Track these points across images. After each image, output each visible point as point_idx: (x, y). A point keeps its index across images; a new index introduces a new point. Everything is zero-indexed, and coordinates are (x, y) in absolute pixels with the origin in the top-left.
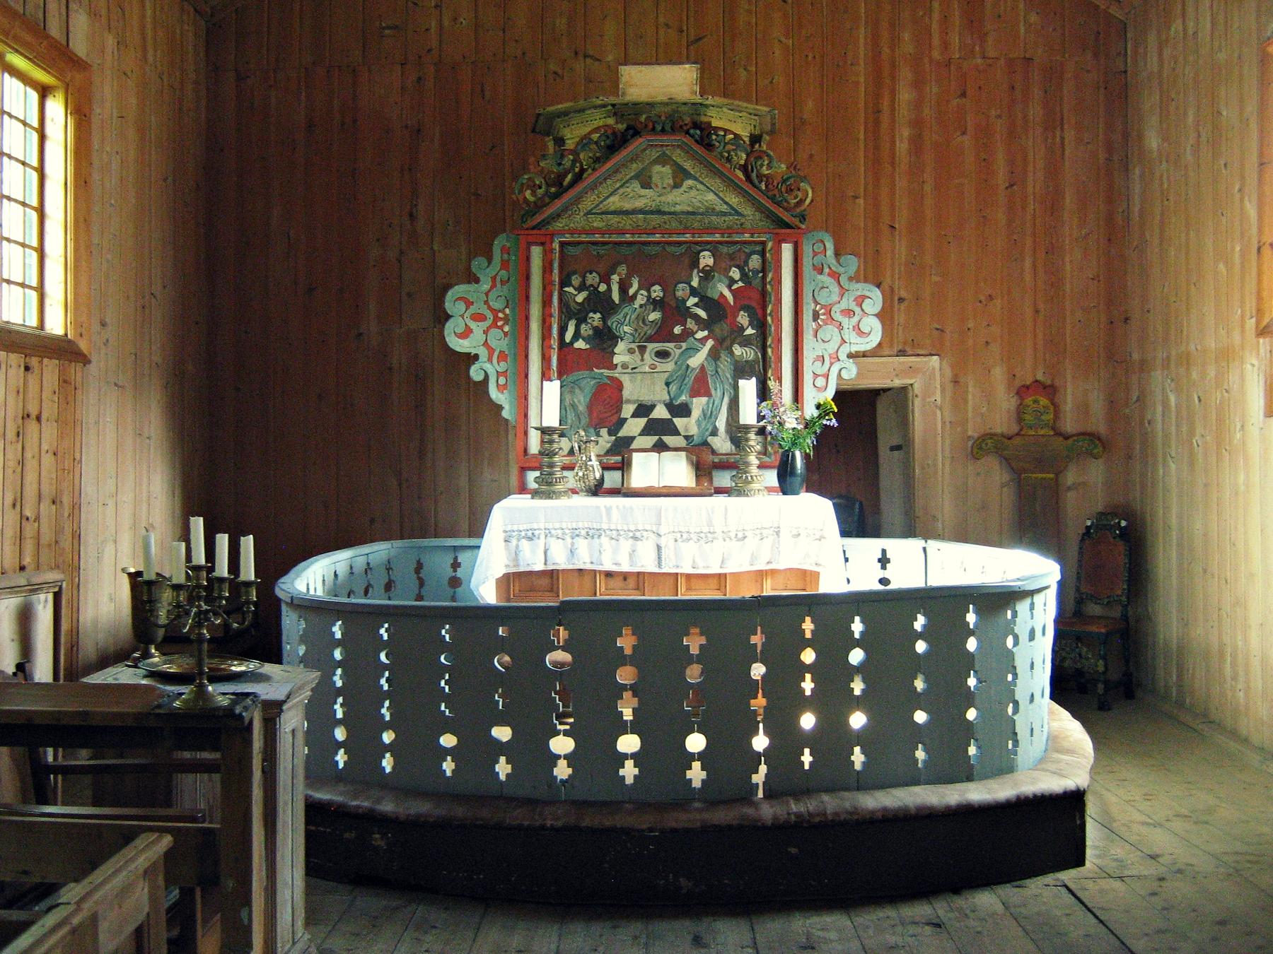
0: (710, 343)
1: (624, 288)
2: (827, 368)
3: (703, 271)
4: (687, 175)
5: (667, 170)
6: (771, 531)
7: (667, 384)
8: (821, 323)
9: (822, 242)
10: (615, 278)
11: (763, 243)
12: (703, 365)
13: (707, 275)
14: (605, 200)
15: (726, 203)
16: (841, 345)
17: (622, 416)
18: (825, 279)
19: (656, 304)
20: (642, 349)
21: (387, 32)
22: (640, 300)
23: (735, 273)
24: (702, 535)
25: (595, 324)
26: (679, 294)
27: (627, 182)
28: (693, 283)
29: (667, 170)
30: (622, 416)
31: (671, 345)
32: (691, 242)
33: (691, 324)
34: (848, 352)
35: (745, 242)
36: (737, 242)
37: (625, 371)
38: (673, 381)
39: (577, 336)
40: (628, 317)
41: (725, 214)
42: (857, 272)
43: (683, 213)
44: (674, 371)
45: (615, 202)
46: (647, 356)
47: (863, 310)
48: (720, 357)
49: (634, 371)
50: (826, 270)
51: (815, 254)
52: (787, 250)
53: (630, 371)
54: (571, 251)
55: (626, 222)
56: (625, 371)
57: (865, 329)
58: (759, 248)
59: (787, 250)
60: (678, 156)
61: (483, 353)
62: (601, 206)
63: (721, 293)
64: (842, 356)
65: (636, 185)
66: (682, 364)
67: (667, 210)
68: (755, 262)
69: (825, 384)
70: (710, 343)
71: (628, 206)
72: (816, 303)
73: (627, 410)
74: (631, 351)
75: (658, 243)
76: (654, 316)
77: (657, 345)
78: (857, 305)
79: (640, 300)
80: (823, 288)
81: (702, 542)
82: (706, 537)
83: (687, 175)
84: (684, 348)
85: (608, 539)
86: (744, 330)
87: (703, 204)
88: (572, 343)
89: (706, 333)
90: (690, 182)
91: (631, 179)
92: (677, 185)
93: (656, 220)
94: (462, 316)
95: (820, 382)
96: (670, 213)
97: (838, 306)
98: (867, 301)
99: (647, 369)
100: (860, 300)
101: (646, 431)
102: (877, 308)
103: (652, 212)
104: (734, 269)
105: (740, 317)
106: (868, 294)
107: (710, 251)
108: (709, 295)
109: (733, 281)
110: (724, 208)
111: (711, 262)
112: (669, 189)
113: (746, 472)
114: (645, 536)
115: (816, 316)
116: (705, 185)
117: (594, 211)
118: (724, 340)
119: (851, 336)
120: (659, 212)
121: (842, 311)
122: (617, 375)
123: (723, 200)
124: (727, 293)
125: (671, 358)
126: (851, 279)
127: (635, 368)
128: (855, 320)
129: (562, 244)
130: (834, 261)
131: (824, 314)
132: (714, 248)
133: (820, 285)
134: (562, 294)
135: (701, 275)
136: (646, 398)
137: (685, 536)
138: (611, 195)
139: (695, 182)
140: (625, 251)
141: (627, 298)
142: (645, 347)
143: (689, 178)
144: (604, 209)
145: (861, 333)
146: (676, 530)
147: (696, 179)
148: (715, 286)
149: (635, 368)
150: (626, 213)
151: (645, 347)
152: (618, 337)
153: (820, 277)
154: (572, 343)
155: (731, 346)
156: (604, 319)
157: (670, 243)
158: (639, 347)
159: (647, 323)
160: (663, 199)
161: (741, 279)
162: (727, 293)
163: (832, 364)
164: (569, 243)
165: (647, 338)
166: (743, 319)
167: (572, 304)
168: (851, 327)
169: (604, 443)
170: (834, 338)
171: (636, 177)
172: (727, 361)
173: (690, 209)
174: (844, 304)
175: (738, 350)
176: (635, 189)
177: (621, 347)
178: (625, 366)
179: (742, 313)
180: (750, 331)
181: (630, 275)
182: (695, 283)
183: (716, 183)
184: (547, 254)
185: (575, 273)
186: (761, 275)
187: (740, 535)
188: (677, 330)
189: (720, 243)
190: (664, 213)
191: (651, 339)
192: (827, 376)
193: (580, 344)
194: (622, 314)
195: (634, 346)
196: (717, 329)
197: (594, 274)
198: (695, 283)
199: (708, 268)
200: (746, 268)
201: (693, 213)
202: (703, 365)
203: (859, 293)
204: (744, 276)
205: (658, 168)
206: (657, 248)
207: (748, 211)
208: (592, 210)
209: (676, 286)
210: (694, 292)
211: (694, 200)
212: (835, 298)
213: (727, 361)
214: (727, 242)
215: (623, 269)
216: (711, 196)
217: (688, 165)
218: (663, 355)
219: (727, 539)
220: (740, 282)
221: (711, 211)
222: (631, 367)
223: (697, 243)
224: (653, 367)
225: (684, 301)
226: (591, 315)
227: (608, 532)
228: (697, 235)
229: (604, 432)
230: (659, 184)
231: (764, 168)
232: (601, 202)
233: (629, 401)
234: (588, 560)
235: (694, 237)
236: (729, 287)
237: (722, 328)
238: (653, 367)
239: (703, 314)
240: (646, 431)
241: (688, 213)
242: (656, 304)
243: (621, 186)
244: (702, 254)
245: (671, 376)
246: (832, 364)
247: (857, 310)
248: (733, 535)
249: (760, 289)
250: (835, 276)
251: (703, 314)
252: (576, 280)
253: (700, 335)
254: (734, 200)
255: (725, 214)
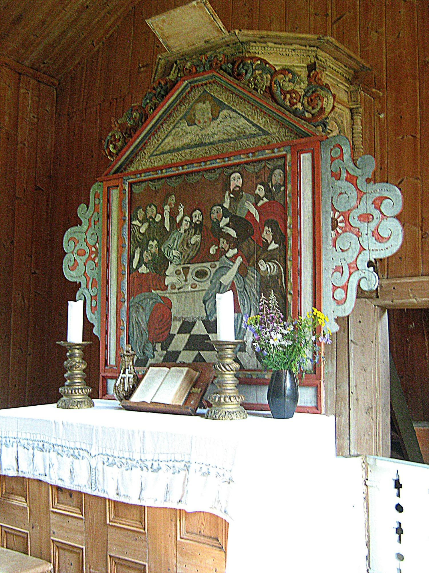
0: (239, 260)
1: (173, 218)
2: (346, 280)
3: (233, 192)
4: (222, 106)
5: (207, 105)
6: (181, 465)
7: (205, 302)
8: (340, 231)
9: (340, 146)
10: (167, 208)
11: (284, 157)
12: (233, 282)
13: (237, 196)
14: (162, 142)
15: (254, 125)
16: (360, 253)
17: (171, 333)
18: (343, 184)
19: (196, 228)
20: (186, 270)
21: (142, 69)
22: (185, 226)
23: (260, 191)
24: (124, 461)
25: (153, 250)
26: (214, 216)
27: (178, 122)
28: (225, 205)
29: (207, 105)
30: (171, 333)
31: (208, 265)
32: (223, 167)
33: (223, 243)
34: (367, 260)
35: (268, 159)
36: (260, 161)
37: (174, 291)
38: (210, 298)
39: (140, 264)
40: (176, 242)
41: (253, 136)
42: (374, 174)
43: (219, 141)
44: (210, 288)
45: (169, 142)
46: (189, 276)
47: (381, 212)
48: (247, 273)
49: (181, 290)
50: (344, 175)
51: (333, 160)
52: (306, 159)
53: (176, 291)
54: (136, 189)
55: (176, 158)
56: (174, 291)
57: (384, 234)
58: (280, 163)
59: (306, 159)
60: (215, 91)
61: (83, 280)
62: (160, 147)
63: (249, 211)
64: (362, 264)
65: (184, 124)
66: (215, 283)
67: (207, 141)
68: (277, 176)
69: (344, 296)
70: (239, 260)
71: (179, 144)
72: (334, 210)
73: (176, 326)
74: (178, 273)
75: (198, 172)
76: (195, 239)
77: (197, 265)
78: (375, 208)
79: (185, 226)
80: (341, 194)
81: (124, 468)
82: (127, 463)
83: (222, 106)
84: (217, 267)
85: (55, 453)
86: (268, 245)
87: (235, 130)
88: (137, 269)
89: (236, 251)
90: (225, 112)
91: (181, 119)
92: (215, 118)
93: (199, 152)
94: (72, 252)
95: (340, 294)
96: (210, 144)
97: (356, 210)
98: (385, 202)
99: (190, 289)
100: (378, 203)
101: (188, 347)
102: (398, 209)
103: (196, 146)
104: (259, 186)
105: (265, 233)
106: (386, 194)
107: (239, 172)
108: (238, 214)
109: (258, 198)
110: (253, 130)
111: (240, 182)
112: (208, 123)
113: (220, 393)
114: (82, 455)
115: (334, 225)
116: (237, 112)
117: (155, 153)
118: (251, 257)
119: (370, 243)
120: (202, 144)
121: (360, 217)
122: (167, 295)
123: (251, 122)
124: (253, 211)
125: (208, 277)
126: (368, 181)
127: (180, 288)
128: (373, 225)
129: (131, 185)
130: (351, 164)
131: (342, 222)
132: (241, 168)
133: (339, 191)
134: (130, 226)
135: (232, 196)
136: (189, 316)
137: (111, 459)
138: (167, 136)
139: (229, 111)
140: (174, 183)
141: (175, 225)
142: (188, 268)
143: (224, 109)
144: (161, 151)
145: (380, 239)
146: (104, 453)
147: (231, 109)
148: (243, 204)
149: (180, 288)
150: (178, 150)
151: (188, 268)
152: (168, 261)
153: (338, 183)
154: (137, 269)
155: (257, 262)
156: (159, 246)
157: (206, 170)
158: (183, 268)
159: (190, 245)
160: (203, 132)
161: (265, 196)
162: (253, 211)
163: (350, 274)
164: (134, 183)
165: (190, 260)
166: (267, 234)
167: (137, 234)
168: (370, 233)
169: (159, 357)
170: (353, 246)
171: (184, 117)
172: (254, 277)
173: (225, 137)
174: (362, 209)
175: (263, 266)
176: (184, 128)
177: (171, 269)
178: (173, 287)
179: (266, 228)
180: (273, 246)
181: (177, 205)
182: (226, 205)
183: (245, 109)
184: (122, 193)
185: (139, 208)
186: (282, 189)
187: (155, 467)
188: (212, 250)
189: (247, 163)
190: (205, 145)
191: (191, 261)
192: (345, 288)
193: (143, 269)
194: (172, 240)
195: (180, 268)
196: (244, 245)
197: (153, 207)
198: (226, 205)
199: (238, 189)
200: (270, 184)
201: (228, 140)
202: (233, 282)
203: (377, 195)
204: (268, 191)
205: (200, 105)
206: (198, 177)
207: (273, 129)
208: (153, 153)
209: (211, 210)
210: (226, 213)
211: (228, 128)
212: (354, 203)
213: (254, 277)
214: (253, 162)
215: (172, 200)
216: (242, 121)
217: (223, 98)
218: (201, 274)
219: (145, 468)
220: (264, 199)
221: (242, 135)
222: (177, 287)
223: (227, 167)
224: (194, 286)
225: (219, 222)
226: (151, 242)
227: (56, 447)
228: (232, 158)
229: (158, 346)
230: (202, 121)
231: (297, 88)
232: (160, 144)
233: (176, 319)
234: (42, 473)
235: (224, 161)
236: (255, 205)
237: (249, 245)
238: (194, 286)
239: (233, 233)
240: (188, 347)
241: (224, 141)
242: (196, 228)
243: (174, 128)
244: (232, 176)
245: (208, 294)
246: (350, 274)
247: (376, 213)
248: (149, 465)
249: (282, 202)
250: (352, 179)
251: (233, 233)
252: (140, 214)
253: (231, 253)
254: (261, 121)
255: (253, 136)
